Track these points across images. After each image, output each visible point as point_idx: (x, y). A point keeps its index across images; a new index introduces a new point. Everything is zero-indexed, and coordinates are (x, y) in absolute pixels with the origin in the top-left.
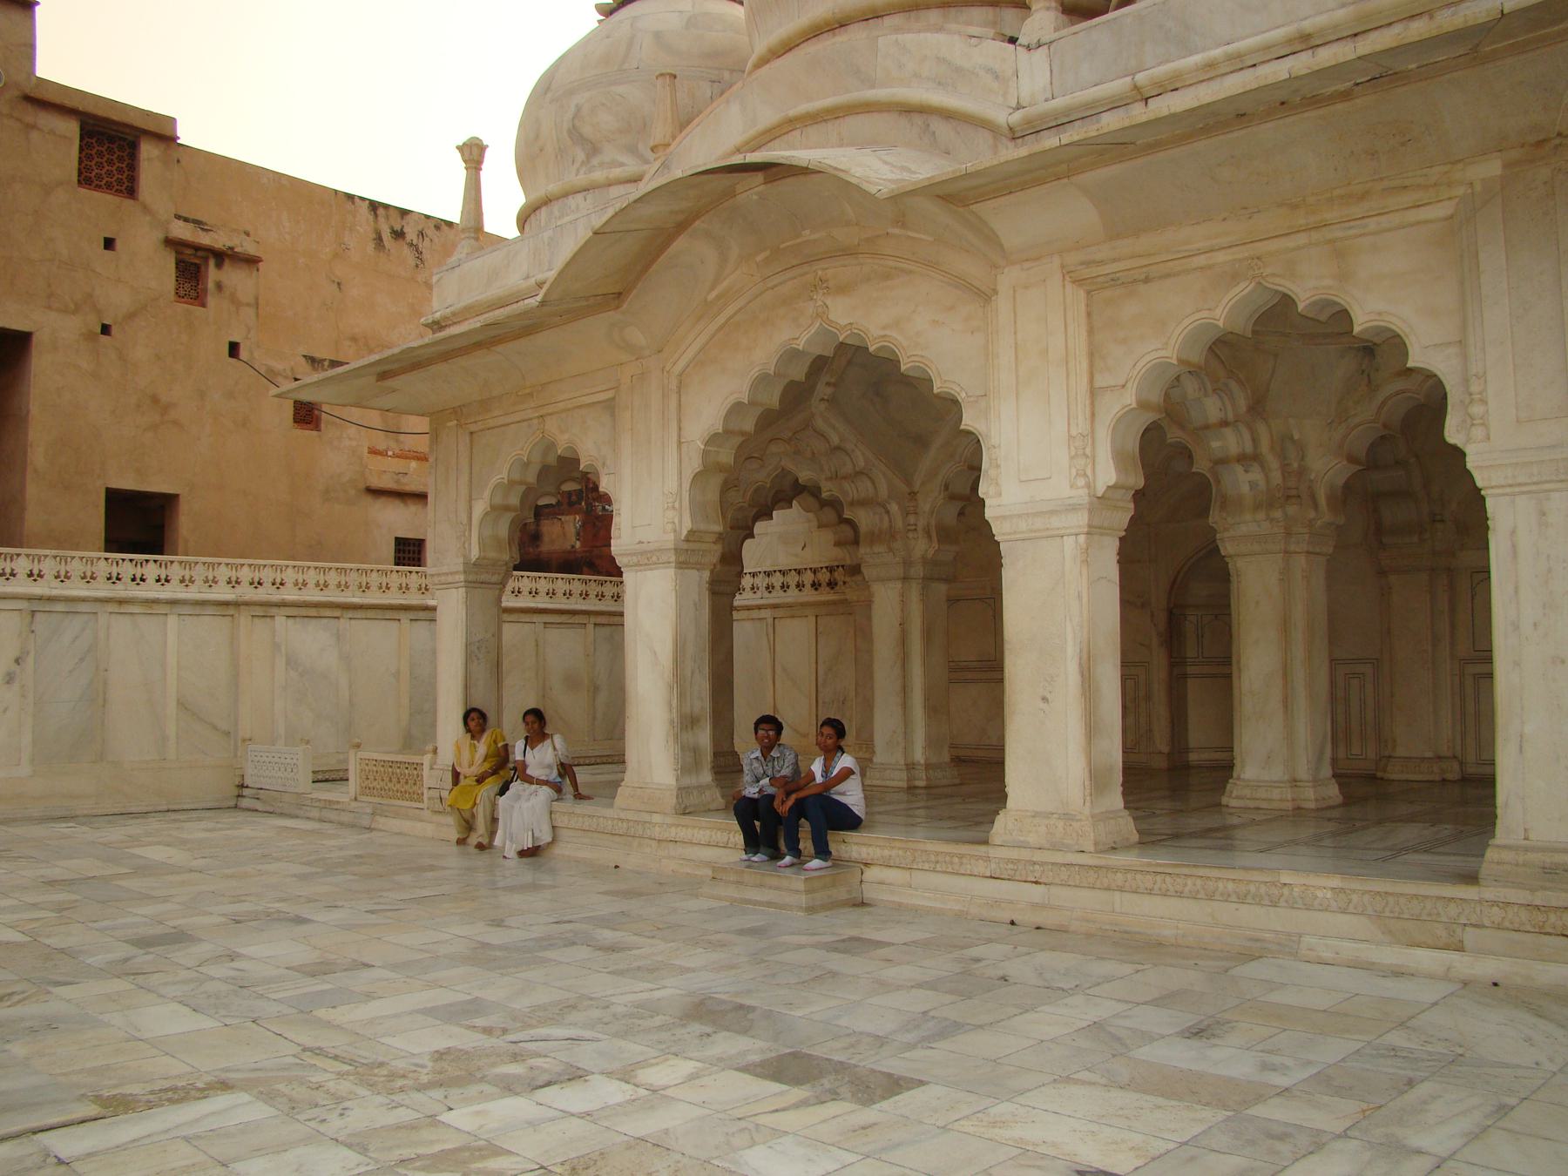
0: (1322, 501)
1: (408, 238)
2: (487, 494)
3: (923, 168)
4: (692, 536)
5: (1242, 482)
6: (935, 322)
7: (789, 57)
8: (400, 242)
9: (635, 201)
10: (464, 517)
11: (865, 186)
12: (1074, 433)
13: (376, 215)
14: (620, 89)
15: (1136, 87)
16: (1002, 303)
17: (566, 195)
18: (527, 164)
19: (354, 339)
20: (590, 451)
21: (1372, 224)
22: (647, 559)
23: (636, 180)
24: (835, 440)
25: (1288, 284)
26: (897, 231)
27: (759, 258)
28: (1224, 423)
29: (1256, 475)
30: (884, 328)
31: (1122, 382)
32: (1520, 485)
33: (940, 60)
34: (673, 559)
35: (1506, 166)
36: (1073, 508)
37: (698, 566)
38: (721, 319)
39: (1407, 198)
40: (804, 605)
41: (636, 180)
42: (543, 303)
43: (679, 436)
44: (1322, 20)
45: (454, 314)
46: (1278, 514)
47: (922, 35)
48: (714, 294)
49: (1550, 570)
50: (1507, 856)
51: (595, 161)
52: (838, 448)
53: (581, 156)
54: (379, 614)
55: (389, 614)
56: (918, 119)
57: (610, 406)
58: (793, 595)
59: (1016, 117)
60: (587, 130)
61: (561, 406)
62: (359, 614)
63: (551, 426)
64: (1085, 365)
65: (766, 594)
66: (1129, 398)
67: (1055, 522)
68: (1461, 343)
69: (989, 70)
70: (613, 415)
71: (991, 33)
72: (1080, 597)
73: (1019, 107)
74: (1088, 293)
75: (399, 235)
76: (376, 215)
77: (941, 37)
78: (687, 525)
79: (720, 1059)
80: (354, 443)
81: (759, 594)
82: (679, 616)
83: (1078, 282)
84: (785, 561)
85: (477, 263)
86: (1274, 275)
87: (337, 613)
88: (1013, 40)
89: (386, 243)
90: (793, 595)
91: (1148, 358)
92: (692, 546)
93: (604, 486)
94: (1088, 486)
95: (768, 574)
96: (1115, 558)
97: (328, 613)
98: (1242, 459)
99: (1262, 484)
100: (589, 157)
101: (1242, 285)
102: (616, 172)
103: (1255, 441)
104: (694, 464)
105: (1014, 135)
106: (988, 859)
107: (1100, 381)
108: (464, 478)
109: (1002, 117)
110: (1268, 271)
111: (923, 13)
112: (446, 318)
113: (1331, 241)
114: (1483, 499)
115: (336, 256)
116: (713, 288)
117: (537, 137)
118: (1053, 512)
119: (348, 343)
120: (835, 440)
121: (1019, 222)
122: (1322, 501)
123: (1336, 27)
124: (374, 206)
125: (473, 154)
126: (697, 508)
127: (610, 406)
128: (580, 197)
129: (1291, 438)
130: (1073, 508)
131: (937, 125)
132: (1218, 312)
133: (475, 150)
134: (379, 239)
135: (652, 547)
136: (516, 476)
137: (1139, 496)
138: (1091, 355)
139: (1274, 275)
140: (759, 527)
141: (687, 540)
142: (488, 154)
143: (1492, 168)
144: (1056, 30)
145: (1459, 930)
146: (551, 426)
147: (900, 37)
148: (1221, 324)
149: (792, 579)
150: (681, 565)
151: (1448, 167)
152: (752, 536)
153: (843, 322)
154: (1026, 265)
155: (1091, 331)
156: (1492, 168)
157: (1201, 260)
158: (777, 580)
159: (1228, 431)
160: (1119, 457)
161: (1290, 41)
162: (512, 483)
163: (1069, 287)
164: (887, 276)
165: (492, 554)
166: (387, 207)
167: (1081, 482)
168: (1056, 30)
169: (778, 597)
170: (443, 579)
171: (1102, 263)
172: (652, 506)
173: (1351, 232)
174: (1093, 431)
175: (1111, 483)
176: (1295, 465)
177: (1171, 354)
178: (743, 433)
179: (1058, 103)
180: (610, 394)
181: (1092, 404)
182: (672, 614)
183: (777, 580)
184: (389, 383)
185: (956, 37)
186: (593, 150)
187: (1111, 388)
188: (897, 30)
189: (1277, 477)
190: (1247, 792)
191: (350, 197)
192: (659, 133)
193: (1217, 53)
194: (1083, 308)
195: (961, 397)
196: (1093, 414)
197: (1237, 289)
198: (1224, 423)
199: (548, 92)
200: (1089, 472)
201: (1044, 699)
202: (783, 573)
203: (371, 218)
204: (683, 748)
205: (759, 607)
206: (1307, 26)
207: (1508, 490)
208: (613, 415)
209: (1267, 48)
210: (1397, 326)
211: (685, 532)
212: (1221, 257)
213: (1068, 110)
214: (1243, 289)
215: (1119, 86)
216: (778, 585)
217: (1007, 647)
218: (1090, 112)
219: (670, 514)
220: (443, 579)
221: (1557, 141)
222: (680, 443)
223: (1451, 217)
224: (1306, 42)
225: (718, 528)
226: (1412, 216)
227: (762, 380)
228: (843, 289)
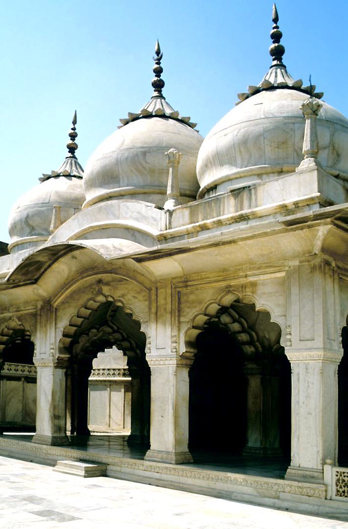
30: (120, 297)
32: (301, 360)
37: (62, 368)
49: (308, 386)
50: (293, 471)
51: (33, 233)
60: (31, 222)
69: (153, 218)
71: (154, 205)
72: (173, 386)
79: (26, 510)
86: (233, 290)
96: (187, 375)
106: (143, 465)
114: (290, 364)
129: (265, 337)
139: (233, 290)
140: (99, 354)
144: (174, 206)
145: (278, 493)
151: (283, 261)
175: (184, 351)
182: (52, 382)
187: (185, 322)
190: (248, 450)
200: (177, 347)
201: (162, 417)
204: (54, 425)
210: (268, 309)
216: (101, 374)
217: (152, 400)
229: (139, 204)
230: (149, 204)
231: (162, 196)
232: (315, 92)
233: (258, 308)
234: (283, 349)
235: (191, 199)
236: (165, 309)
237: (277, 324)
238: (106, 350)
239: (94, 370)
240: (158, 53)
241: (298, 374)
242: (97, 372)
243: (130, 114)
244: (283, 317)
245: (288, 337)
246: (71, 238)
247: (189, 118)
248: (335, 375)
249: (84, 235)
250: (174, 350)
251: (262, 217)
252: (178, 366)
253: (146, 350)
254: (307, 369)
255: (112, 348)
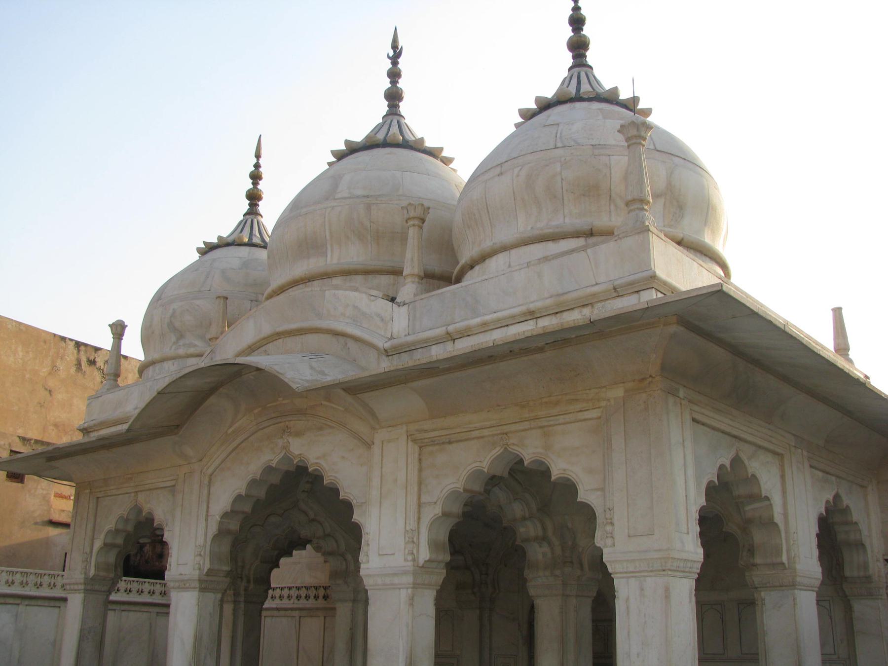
0: (586, 566)
1: (98, 365)
2: (102, 536)
3: (335, 372)
4: (210, 572)
5: (538, 553)
6: (343, 457)
7: (282, 296)
8: (93, 367)
9: (180, 378)
10: (88, 550)
11: (291, 384)
12: (408, 528)
13: (79, 351)
14: (198, 302)
15: (448, 333)
16: (376, 449)
17: (162, 360)
18: (147, 339)
19: (56, 425)
20: (160, 514)
21: (561, 419)
22: (183, 586)
23: (200, 355)
24: (312, 515)
25: (520, 450)
26: (324, 403)
27: (256, 411)
28: (524, 519)
29: (545, 548)
30: (317, 458)
31: (435, 500)
33: (355, 307)
34: (198, 586)
35: (626, 391)
36: (405, 573)
38: (234, 444)
39: (578, 406)
40: (317, 609)
41: (200, 355)
42: (128, 430)
43: (207, 511)
44: (539, 304)
45: (95, 425)
46: (558, 572)
47: (347, 292)
48: (231, 430)
51: (181, 343)
52: (313, 520)
53: (174, 339)
54: (46, 603)
55: (52, 603)
56: (341, 338)
57: (172, 489)
58: (312, 603)
59: (387, 345)
60: (177, 324)
61: (147, 487)
62: (33, 602)
63: (141, 498)
64: (416, 489)
65: (296, 601)
66: (438, 510)
67: (396, 580)
68: (602, 489)
69: (378, 315)
70: (174, 495)
73: (392, 338)
74: (420, 447)
75: (92, 363)
76: (79, 351)
77: (356, 294)
78: (207, 566)
80: (45, 492)
81: (292, 601)
82: (199, 622)
83: (414, 441)
84: (308, 580)
85: (111, 396)
86: (514, 444)
87: (18, 601)
88: (393, 300)
89: (83, 367)
90: (312, 603)
91: (449, 487)
92: (210, 578)
93: (166, 538)
94: (414, 560)
95: (298, 588)
97: (11, 601)
98: (536, 539)
99: (549, 555)
100: (178, 339)
101: (498, 449)
102: (192, 350)
103: (544, 528)
104: (213, 529)
105: (387, 353)
107: (424, 499)
108: (90, 526)
109: (381, 344)
110: (511, 441)
111: (353, 277)
112: (91, 427)
113: (541, 427)
114: (612, 580)
115: (50, 374)
116: (230, 427)
117: (151, 326)
118: (395, 574)
119: (52, 428)
120: (312, 515)
121: (387, 404)
122: (586, 566)
123: (546, 308)
124: (78, 344)
125: (118, 329)
126: (214, 556)
127: (172, 489)
128: (170, 362)
130: (405, 573)
131: (351, 344)
132: (485, 463)
133: (119, 328)
134: (79, 364)
135: (186, 578)
136: (121, 526)
137: (451, 567)
138: (420, 484)
140: (283, 561)
141: (207, 574)
142: (127, 330)
143: (618, 392)
146: (141, 498)
147: (337, 292)
148: (486, 470)
149: (312, 593)
150: (202, 590)
152: (278, 566)
153: (297, 453)
154: (390, 429)
155: (420, 470)
156: (618, 392)
157: (476, 434)
158: (303, 593)
159: (528, 523)
160: (434, 545)
161: (524, 314)
162: (117, 531)
163: (410, 443)
164: (320, 429)
165: (102, 574)
166: (86, 345)
167: (410, 558)
168: (415, 295)
169: (303, 603)
170: (72, 587)
171: (426, 431)
172: (189, 551)
173: (552, 423)
174: (419, 528)
175: (427, 559)
176: (570, 543)
177: (460, 486)
178: (243, 512)
179: (410, 339)
180: (173, 483)
181: (419, 512)
183: (294, 593)
184: (53, 463)
185: (364, 296)
186: (181, 336)
188: (337, 287)
189: (558, 551)
191: (63, 339)
192: (213, 331)
193: (488, 318)
194: (417, 455)
195: (354, 502)
196: (419, 518)
197: (494, 452)
198: (524, 519)
199: (160, 300)
200: (415, 552)
202: (307, 588)
203: (75, 352)
205: (292, 609)
206: (532, 307)
207: (625, 575)
208: (174, 495)
209: (513, 317)
210: (573, 477)
211: (206, 570)
212: (486, 432)
213: (414, 343)
214: (497, 451)
215: (440, 331)
218: (427, 344)
219: (198, 558)
220: (72, 587)
221: (650, 379)
222: (207, 516)
223: (600, 418)
224: (532, 315)
225: (226, 568)
226: (581, 416)
227: (253, 483)
228: (298, 434)
229: (33, 434)
230: (374, 292)
231: (396, 277)
232: (639, 107)
233: (555, 474)
234: (600, 550)
235: (442, 283)
236: (396, 480)
237: (589, 506)
238: (294, 552)
239: (274, 589)
240: (395, 45)
241: (628, 599)
242: (277, 593)
243: (347, 142)
244: (599, 493)
245: (609, 528)
246: (239, 355)
247: (441, 149)
248: (690, 602)
249: (252, 349)
250: (410, 558)
251: (419, 523)
252: (415, 586)
253: (362, 558)
254: (643, 590)
255: (305, 548)
